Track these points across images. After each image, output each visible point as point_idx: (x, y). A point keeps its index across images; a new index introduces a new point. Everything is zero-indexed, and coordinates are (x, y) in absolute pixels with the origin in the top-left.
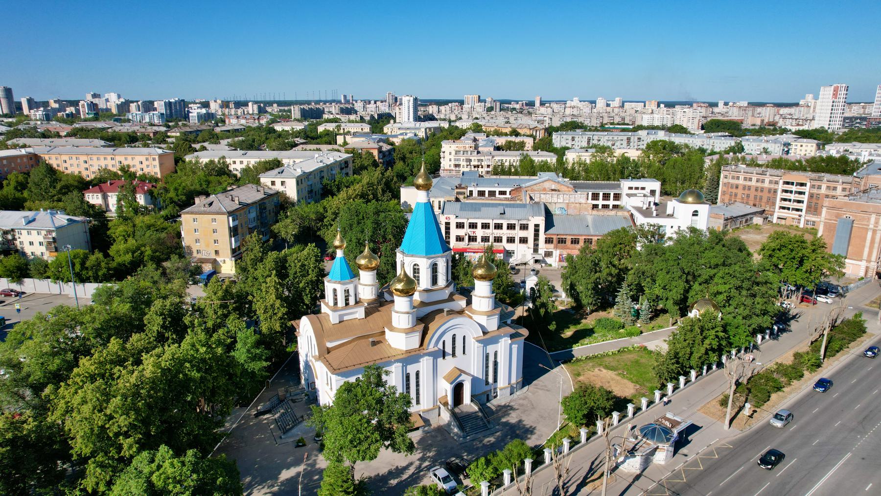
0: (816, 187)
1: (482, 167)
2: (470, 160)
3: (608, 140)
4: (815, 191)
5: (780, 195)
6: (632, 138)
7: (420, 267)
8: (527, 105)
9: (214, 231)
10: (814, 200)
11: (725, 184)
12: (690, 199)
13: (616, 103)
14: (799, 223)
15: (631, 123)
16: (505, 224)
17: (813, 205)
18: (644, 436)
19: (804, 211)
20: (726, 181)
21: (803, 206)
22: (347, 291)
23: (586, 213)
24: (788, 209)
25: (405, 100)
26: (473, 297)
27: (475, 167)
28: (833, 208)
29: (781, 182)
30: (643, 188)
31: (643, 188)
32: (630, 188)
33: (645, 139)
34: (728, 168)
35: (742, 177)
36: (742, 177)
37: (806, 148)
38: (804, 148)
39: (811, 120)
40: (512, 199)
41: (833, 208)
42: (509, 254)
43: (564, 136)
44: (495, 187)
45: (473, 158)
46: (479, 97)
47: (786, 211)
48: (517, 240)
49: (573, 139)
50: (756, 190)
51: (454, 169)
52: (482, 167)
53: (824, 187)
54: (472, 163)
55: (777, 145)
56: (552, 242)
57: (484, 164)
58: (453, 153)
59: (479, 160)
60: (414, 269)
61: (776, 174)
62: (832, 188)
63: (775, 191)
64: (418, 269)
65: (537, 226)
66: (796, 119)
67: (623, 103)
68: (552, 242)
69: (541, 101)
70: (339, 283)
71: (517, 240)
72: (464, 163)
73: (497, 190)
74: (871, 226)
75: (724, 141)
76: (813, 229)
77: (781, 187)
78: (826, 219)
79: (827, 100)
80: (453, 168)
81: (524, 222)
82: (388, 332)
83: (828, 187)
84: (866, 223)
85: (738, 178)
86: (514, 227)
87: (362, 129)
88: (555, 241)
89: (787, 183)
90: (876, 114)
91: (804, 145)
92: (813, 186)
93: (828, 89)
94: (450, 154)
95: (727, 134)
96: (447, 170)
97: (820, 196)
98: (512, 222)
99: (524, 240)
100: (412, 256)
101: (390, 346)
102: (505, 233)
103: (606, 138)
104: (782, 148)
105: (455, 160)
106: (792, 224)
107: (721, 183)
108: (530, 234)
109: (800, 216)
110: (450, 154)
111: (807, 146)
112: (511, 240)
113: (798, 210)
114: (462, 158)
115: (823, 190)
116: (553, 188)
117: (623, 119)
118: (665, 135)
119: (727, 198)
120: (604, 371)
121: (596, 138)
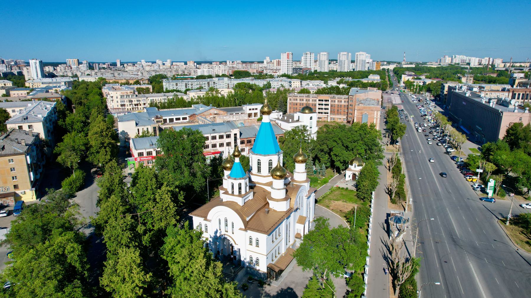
0: (333, 101)
1: (140, 105)
2: (132, 101)
3: (197, 84)
4: (333, 103)
5: (318, 106)
6: (210, 82)
7: (261, 162)
8: (111, 65)
9: (12, 169)
10: (333, 108)
11: (290, 103)
12: (307, 111)
13: (168, 63)
14: (328, 119)
15: (188, 74)
16: (218, 136)
17: (333, 110)
18: (396, 223)
19: (329, 113)
20: (290, 101)
21: (329, 111)
22: (240, 184)
23: (254, 124)
24: (322, 113)
25: (32, 62)
26: (223, 180)
27: (135, 105)
28: (359, 110)
29: (317, 100)
30: (256, 109)
31: (256, 109)
32: (250, 109)
33: (217, 83)
34: (291, 95)
35: (298, 99)
36: (298, 99)
37: (296, 84)
38: (295, 84)
39: (279, 70)
40: (192, 122)
41: (359, 110)
42: (221, 153)
43: (171, 83)
44: (172, 116)
45: (133, 100)
46: (78, 60)
47: (320, 114)
48: (225, 144)
49: (177, 85)
50: (300, 105)
51: (121, 107)
52: (140, 105)
53: (336, 101)
54: (133, 103)
55: (286, 82)
56: (244, 143)
57: (142, 102)
58: (119, 97)
59: (138, 101)
60: (269, 163)
61: (314, 96)
62: (340, 101)
63: (315, 105)
64: (271, 163)
65: (235, 135)
66: (272, 70)
67: (172, 62)
68: (244, 143)
69: (120, 63)
70: (243, 178)
71: (225, 144)
72: (127, 103)
73: (174, 118)
74: (375, 117)
75: (260, 82)
76: (334, 121)
77: (318, 102)
78: (357, 115)
79: (285, 62)
80: (120, 107)
81: (228, 133)
82: (270, 202)
83: (338, 101)
84: (373, 115)
85: (297, 100)
86: (223, 137)
87: (5, 84)
88: (246, 142)
89: (320, 100)
90: (304, 67)
91: (295, 82)
92: (332, 101)
93: (284, 54)
94: (117, 98)
95: (253, 78)
96: (116, 109)
97: (336, 106)
98: (222, 134)
99: (228, 144)
100: (269, 155)
101: (275, 211)
102: (218, 141)
103: (196, 83)
104: (289, 84)
105: (121, 102)
106: (325, 120)
107: (288, 103)
108: (232, 140)
109: (328, 116)
110: (117, 98)
111: (296, 82)
112: (221, 145)
113: (325, 113)
114: (126, 100)
115: (336, 103)
116: (216, 113)
117: (184, 72)
118: (228, 80)
119: (292, 110)
120: (336, 202)
121: (190, 83)
